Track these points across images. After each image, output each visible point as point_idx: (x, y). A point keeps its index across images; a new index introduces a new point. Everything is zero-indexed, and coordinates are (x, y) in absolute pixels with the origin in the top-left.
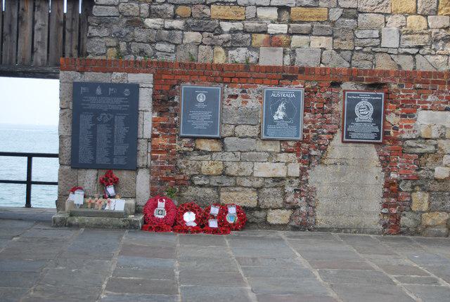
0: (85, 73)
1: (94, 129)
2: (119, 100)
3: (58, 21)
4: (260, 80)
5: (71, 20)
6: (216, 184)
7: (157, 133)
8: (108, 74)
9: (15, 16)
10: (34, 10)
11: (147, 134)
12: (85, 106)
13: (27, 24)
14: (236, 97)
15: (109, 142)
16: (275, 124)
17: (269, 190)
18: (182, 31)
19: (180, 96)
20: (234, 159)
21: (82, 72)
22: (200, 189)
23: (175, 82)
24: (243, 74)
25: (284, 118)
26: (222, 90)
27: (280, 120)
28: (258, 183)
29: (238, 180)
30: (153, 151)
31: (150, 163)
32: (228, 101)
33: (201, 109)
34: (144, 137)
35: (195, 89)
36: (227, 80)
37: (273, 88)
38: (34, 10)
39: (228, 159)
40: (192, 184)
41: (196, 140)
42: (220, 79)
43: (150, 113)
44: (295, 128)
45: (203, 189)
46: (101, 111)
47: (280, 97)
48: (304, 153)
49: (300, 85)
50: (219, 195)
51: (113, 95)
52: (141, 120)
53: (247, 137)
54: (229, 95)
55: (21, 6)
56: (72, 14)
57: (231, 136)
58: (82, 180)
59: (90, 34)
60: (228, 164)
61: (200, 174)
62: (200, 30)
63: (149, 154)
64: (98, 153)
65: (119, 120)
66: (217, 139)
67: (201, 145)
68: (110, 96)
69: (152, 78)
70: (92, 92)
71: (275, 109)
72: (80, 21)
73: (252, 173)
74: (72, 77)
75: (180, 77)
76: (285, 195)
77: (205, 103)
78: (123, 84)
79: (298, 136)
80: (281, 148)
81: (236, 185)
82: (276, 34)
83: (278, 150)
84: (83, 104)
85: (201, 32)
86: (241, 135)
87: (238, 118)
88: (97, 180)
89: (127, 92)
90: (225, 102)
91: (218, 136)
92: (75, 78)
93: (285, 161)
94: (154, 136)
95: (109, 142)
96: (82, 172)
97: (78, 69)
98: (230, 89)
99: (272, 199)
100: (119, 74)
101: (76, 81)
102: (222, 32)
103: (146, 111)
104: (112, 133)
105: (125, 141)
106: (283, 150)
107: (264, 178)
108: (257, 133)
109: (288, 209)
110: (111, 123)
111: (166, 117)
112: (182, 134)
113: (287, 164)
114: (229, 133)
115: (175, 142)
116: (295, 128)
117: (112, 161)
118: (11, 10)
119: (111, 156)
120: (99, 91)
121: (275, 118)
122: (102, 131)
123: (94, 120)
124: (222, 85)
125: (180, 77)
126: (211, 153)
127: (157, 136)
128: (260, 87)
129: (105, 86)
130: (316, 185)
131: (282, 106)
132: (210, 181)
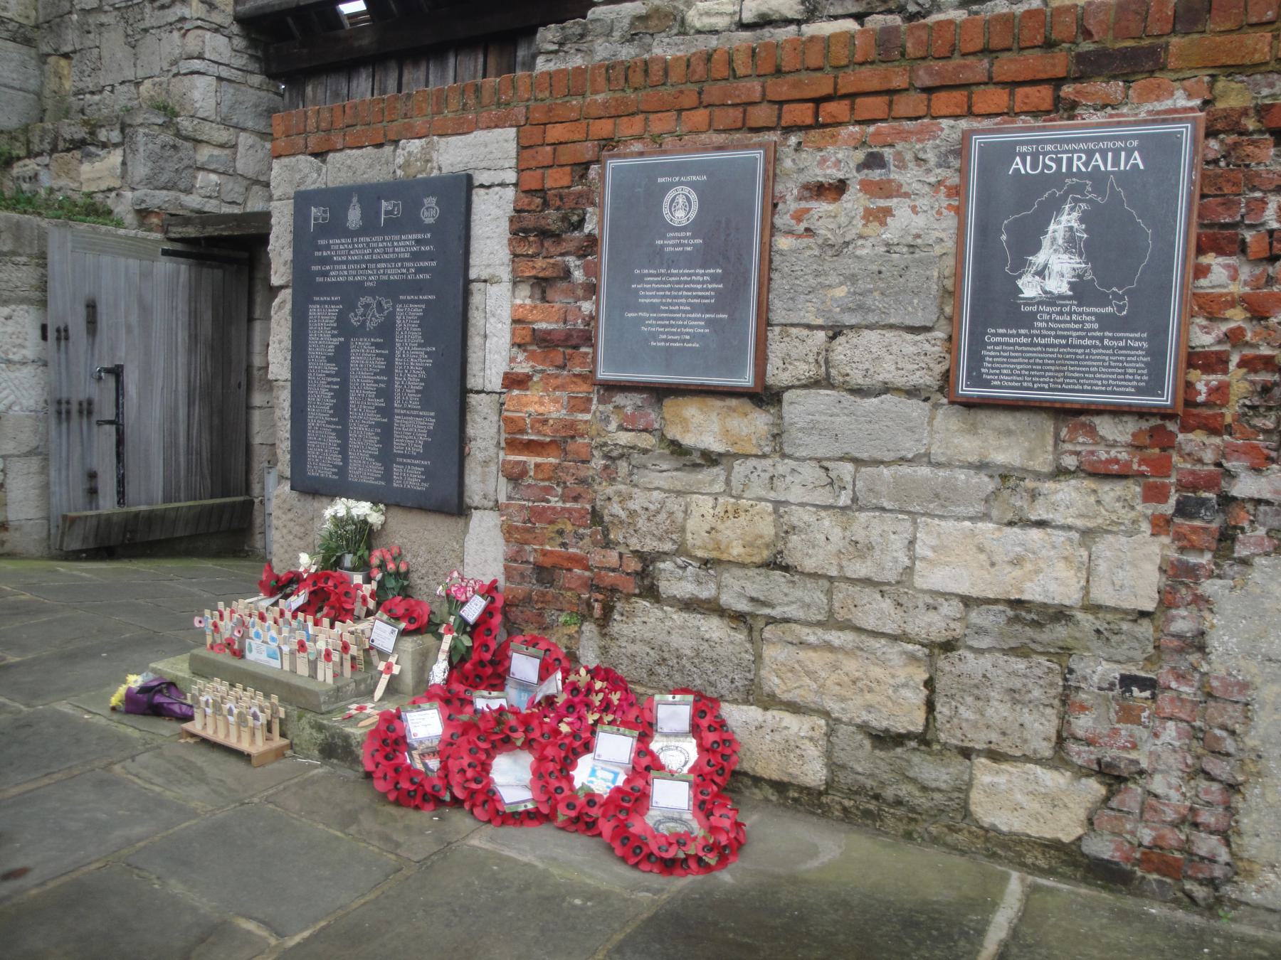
1: (341, 357)
2: (405, 243)
4: (959, 96)
6: (743, 606)
7: (523, 368)
14: (839, 188)
15: (381, 403)
16: (1026, 320)
17: (986, 662)
19: (601, 206)
20: (824, 497)
22: (678, 617)
23: (587, 151)
24: (869, 78)
25: (1081, 291)
26: (773, 160)
27: (1052, 300)
28: (934, 624)
29: (838, 597)
31: (503, 489)
36: (802, 113)
37: (1022, 133)
39: (796, 494)
40: (651, 593)
41: (668, 402)
43: (506, 287)
44: (1138, 341)
45: (695, 620)
46: (359, 289)
47: (1058, 178)
48: (1191, 484)
49: (1181, 101)
50: (758, 658)
51: (395, 226)
53: (886, 389)
54: (806, 187)
57: (815, 384)
60: (800, 516)
64: (353, 444)
65: (409, 315)
67: (685, 423)
69: (512, 147)
70: (335, 227)
71: (1028, 241)
73: (909, 570)
74: (298, 176)
75: (604, 128)
76: (1067, 700)
77: (695, 227)
79: (1155, 386)
80: (1058, 452)
81: (831, 624)
83: (1043, 462)
84: (315, 268)
86: (857, 379)
87: (841, 292)
89: (430, 212)
91: (746, 380)
93: (1079, 523)
94: (513, 381)
95: (381, 403)
98: (808, 158)
99: (999, 711)
100: (415, 145)
101: (303, 188)
104: (389, 371)
106: (1070, 462)
107: (967, 601)
108: (939, 369)
109: (1082, 772)
110: (386, 332)
111: (559, 300)
112: (603, 374)
113: (1088, 535)
114: (804, 370)
115: (585, 405)
116: (1138, 341)
117: (387, 476)
119: (386, 457)
120: (354, 217)
121: (1029, 288)
122: (364, 356)
123: (343, 327)
124: (773, 137)
128: (950, 130)
129: (370, 195)
130: (1251, 669)
131: (1066, 221)
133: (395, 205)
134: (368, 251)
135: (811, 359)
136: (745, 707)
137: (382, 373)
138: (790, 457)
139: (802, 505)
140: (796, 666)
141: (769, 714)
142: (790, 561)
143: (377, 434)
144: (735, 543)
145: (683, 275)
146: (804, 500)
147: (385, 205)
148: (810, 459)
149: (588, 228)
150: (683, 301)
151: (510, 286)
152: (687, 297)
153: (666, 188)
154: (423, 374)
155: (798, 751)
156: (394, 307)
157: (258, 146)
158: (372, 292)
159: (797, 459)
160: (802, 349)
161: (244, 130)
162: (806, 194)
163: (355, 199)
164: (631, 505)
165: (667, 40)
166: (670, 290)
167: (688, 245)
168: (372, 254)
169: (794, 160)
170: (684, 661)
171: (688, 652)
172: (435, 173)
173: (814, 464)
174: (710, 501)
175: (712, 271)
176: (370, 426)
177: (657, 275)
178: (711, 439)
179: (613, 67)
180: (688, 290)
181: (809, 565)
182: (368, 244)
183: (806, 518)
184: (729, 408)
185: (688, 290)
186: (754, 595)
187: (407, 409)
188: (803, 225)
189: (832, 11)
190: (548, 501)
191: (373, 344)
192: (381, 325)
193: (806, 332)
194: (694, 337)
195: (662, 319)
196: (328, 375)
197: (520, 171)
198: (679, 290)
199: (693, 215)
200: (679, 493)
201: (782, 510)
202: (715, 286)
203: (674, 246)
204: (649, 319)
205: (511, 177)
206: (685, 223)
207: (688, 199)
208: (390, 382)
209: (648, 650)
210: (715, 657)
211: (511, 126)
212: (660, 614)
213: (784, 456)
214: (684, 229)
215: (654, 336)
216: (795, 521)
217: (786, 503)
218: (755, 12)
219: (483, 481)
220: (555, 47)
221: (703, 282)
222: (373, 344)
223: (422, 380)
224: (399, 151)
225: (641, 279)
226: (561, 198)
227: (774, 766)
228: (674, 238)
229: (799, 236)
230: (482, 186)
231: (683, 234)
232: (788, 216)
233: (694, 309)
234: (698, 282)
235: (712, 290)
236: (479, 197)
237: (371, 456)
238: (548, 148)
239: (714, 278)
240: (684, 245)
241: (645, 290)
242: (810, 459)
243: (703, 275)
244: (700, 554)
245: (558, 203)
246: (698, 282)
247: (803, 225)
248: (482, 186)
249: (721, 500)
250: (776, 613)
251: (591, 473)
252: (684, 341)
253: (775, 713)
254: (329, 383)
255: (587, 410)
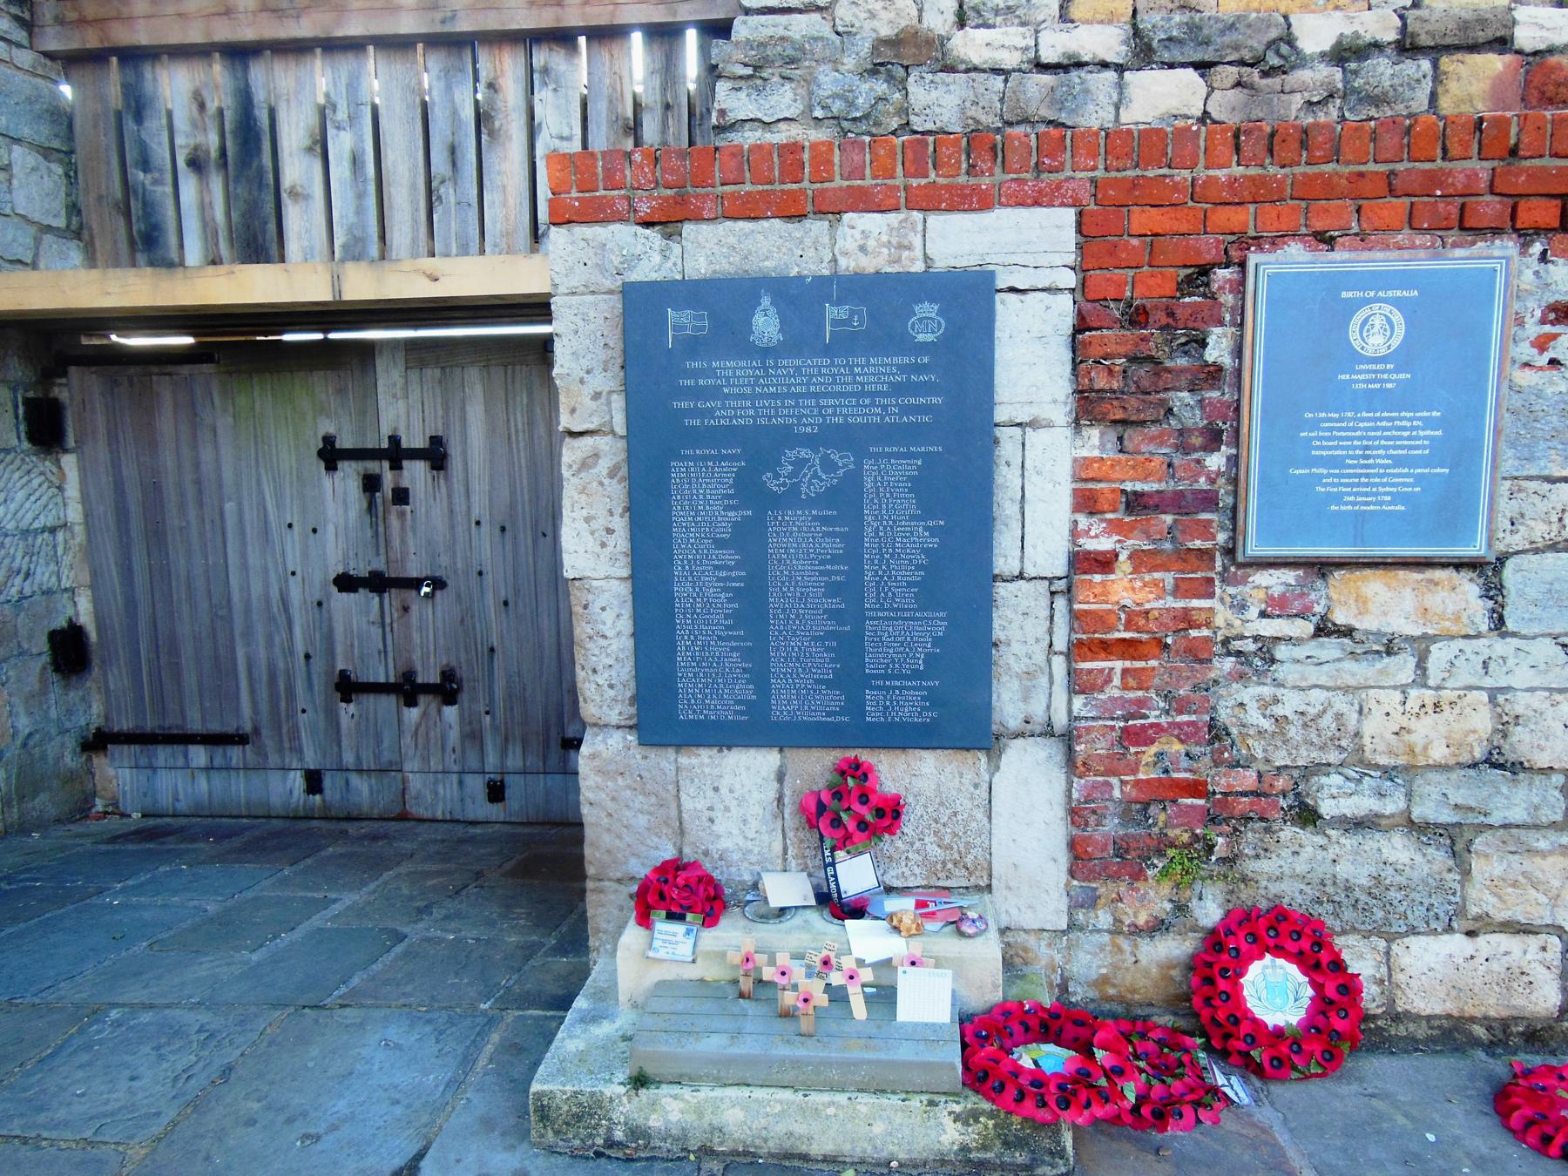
0: (688, 229)
2: (878, 370)
3: (616, 119)
5: (659, 111)
6: (1447, 817)
8: (817, 227)
9: (468, 114)
10: (531, 89)
11: (1050, 556)
12: (692, 413)
13: (510, 138)
15: (834, 603)
18: (1120, 69)
21: (666, 222)
22: (1349, 842)
23: (1208, 245)
30: (1078, 650)
32: (1542, 344)
33: (1373, 399)
34: (1030, 571)
35: (1336, 281)
38: (531, 89)
40: (1307, 816)
42: (1490, 207)
45: (1373, 842)
46: (786, 437)
51: (846, 344)
52: (1007, 478)
55: (483, 75)
56: (664, 90)
58: (701, 805)
59: (722, 113)
60: (1521, 704)
61: (1359, 763)
62: (1198, 56)
63: (1059, 664)
64: (776, 666)
66: (1474, 565)
67: (1362, 603)
68: (828, 351)
69: (1070, 237)
72: (691, 115)
75: (1245, 218)
77: (1402, 358)
78: (905, 278)
82: (1551, 51)
85: (1202, 67)
88: (780, 800)
90: (1526, 351)
91: (1477, 548)
92: (634, 260)
94: (1086, 563)
95: (834, 603)
96: (702, 760)
97: (644, 209)
101: (635, 276)
102: (1302, 61)
103: (1034, 424)
104: (853, 554)
105: (929, 594)
107: (1550, 690)
111: (1153, 447)
115: (1205, 589)
118: (449, 88)
120: (766, 325)
123: (748, 490)
125: (1245, 218)
126: (1421, 646)
127: (1104, 563)
132: (1409, 796)
133: (852, 313)
134: (845, 411)
135: (1554, 518)
136: (1446, 937)
137: (835, 559)
138: (1514, 635)
139: (1531, 690)
140: (1520, 878)
141: (1482, 940)
142: (1512, 757)
143: (828, 650)
144: (1436, 743)
145: (1381, 419)
146: (1535, 684)
147: (832, 312)
148: (1542, 635)
149: (1211, 355)
150: (1381, 452)
151: (1068, 432)
152: (1386, 448)
153: (1355, 306)
154: (923, 559)
155: (1525, 979)
156: (859, 465)
157: (44, 171)
158: (811, 441)
159: (1524, 637)
160: (1543, 506)
161: (17, 141)
162: (1552, 316)
163: (766, 301)
164: (1278, 710)
165: (930, 76)
166: (1360, 438)
167: (1389, 381)
168: (808, 384)
169: (1537, 273)
170: (1358, 894)
171: (1364, 881)
172: (919, 267)
173: (1548, 640)
174: (1398, 696)
175: (1426, 414)
176: (815, 638)
177: (1340, 420)
178: (1402, 621)
179: (1248, 132)
180: (1388, 438)
181: (1542, 760)
182: (798, 369)
183: (1536, 705)
184: (1430, 581)
185: (1388, 438)
186: (1460, 801)
187: (892, 609)
188: (1547, 356)
189: (1166, 56)
190: (1145, 717)
191: (815, 518)
192: (832, 490)
193: (1547, 486)
194: (1397, 498)
195: (1349, 476)
196: (716, 567)
197: (1081, 269)
198: (1375, 438)
199: (1396, 342)
200: (1346, 690)
201: (1501, 699)
202: (1428, 433)
203: (1365, 381)
204: (1329, 475)
205: (1070, 279)
206: (1383, 352)
207: (1389, 321)
208: (856, 573)
209: (1303, 887)
210: (1405, 882)
211: (1063, 205)
212: (1320, 840)
213: (1504, 635)
214: (1383, 360)
215: (1338, 498)
216: (1519, 710)
217: (1509, 689)
218: (1060, 50)
219: (1026, 699)
220: (749, 71)
221: (1412, 428)
222: (815, 518)
223: (919, 567)
224: (843, 230)
225: (1315, 425)
226: (1171, 314)
227: (1492, 1001)
228: (1368, 372)
229: (1541, 368)
230: (1013, 290)
231: (1380, 367)
232: (1527, 344)
233: (1398, 462)
234: (1404, 429)
235: (1425, 438)
236: (1008, 311)
237: (818, 682)
238: (1135, 242)
239: (1428, 423)
240: (1382, 381)
241: (1320, 439)
242: (1542, 635)
243: (1411, 419)
244: (1383, 760)
245: (1164, 320)
246: (1404, 429)
247: (1547, 356)
248: (1013, 290)
249: (1414, 693)
250: (1495, 819)
251: (1212, 675)
252: (1381, 503)
253: (1489, 937)
254: (719, 580)
255: (1211, 595)
